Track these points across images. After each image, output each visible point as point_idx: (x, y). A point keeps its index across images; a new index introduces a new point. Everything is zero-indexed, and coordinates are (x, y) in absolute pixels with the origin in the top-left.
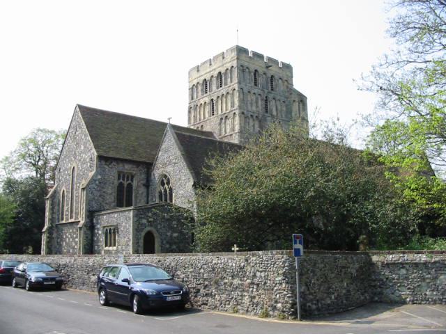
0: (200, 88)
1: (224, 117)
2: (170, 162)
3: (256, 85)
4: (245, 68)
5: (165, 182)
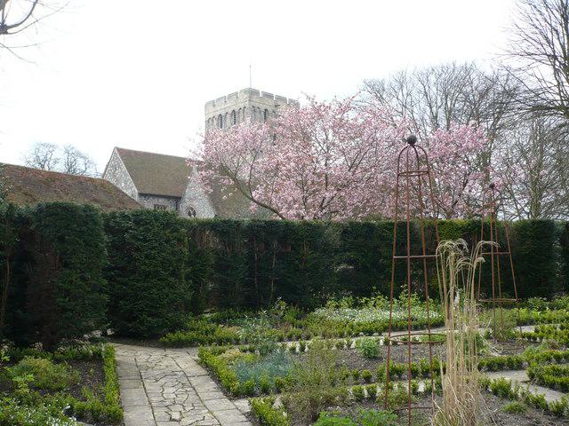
0: (215, 122)
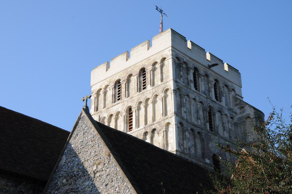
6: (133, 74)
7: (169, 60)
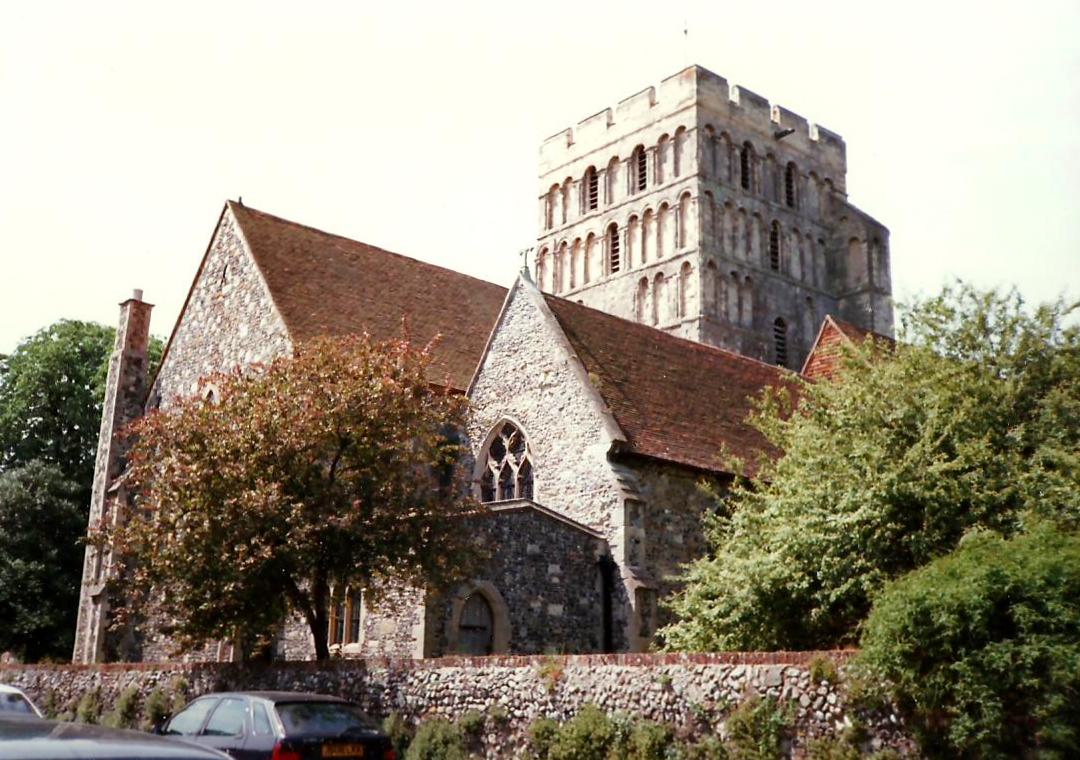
0: (574, 193)
1: (651, 280)
2: (527, 382)
3: (745, 185)
4: (718, 132)
5: (506, 443)
6: (621, 159)
7: (656, 262)
